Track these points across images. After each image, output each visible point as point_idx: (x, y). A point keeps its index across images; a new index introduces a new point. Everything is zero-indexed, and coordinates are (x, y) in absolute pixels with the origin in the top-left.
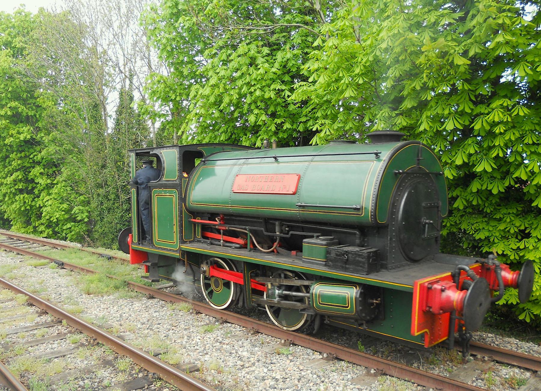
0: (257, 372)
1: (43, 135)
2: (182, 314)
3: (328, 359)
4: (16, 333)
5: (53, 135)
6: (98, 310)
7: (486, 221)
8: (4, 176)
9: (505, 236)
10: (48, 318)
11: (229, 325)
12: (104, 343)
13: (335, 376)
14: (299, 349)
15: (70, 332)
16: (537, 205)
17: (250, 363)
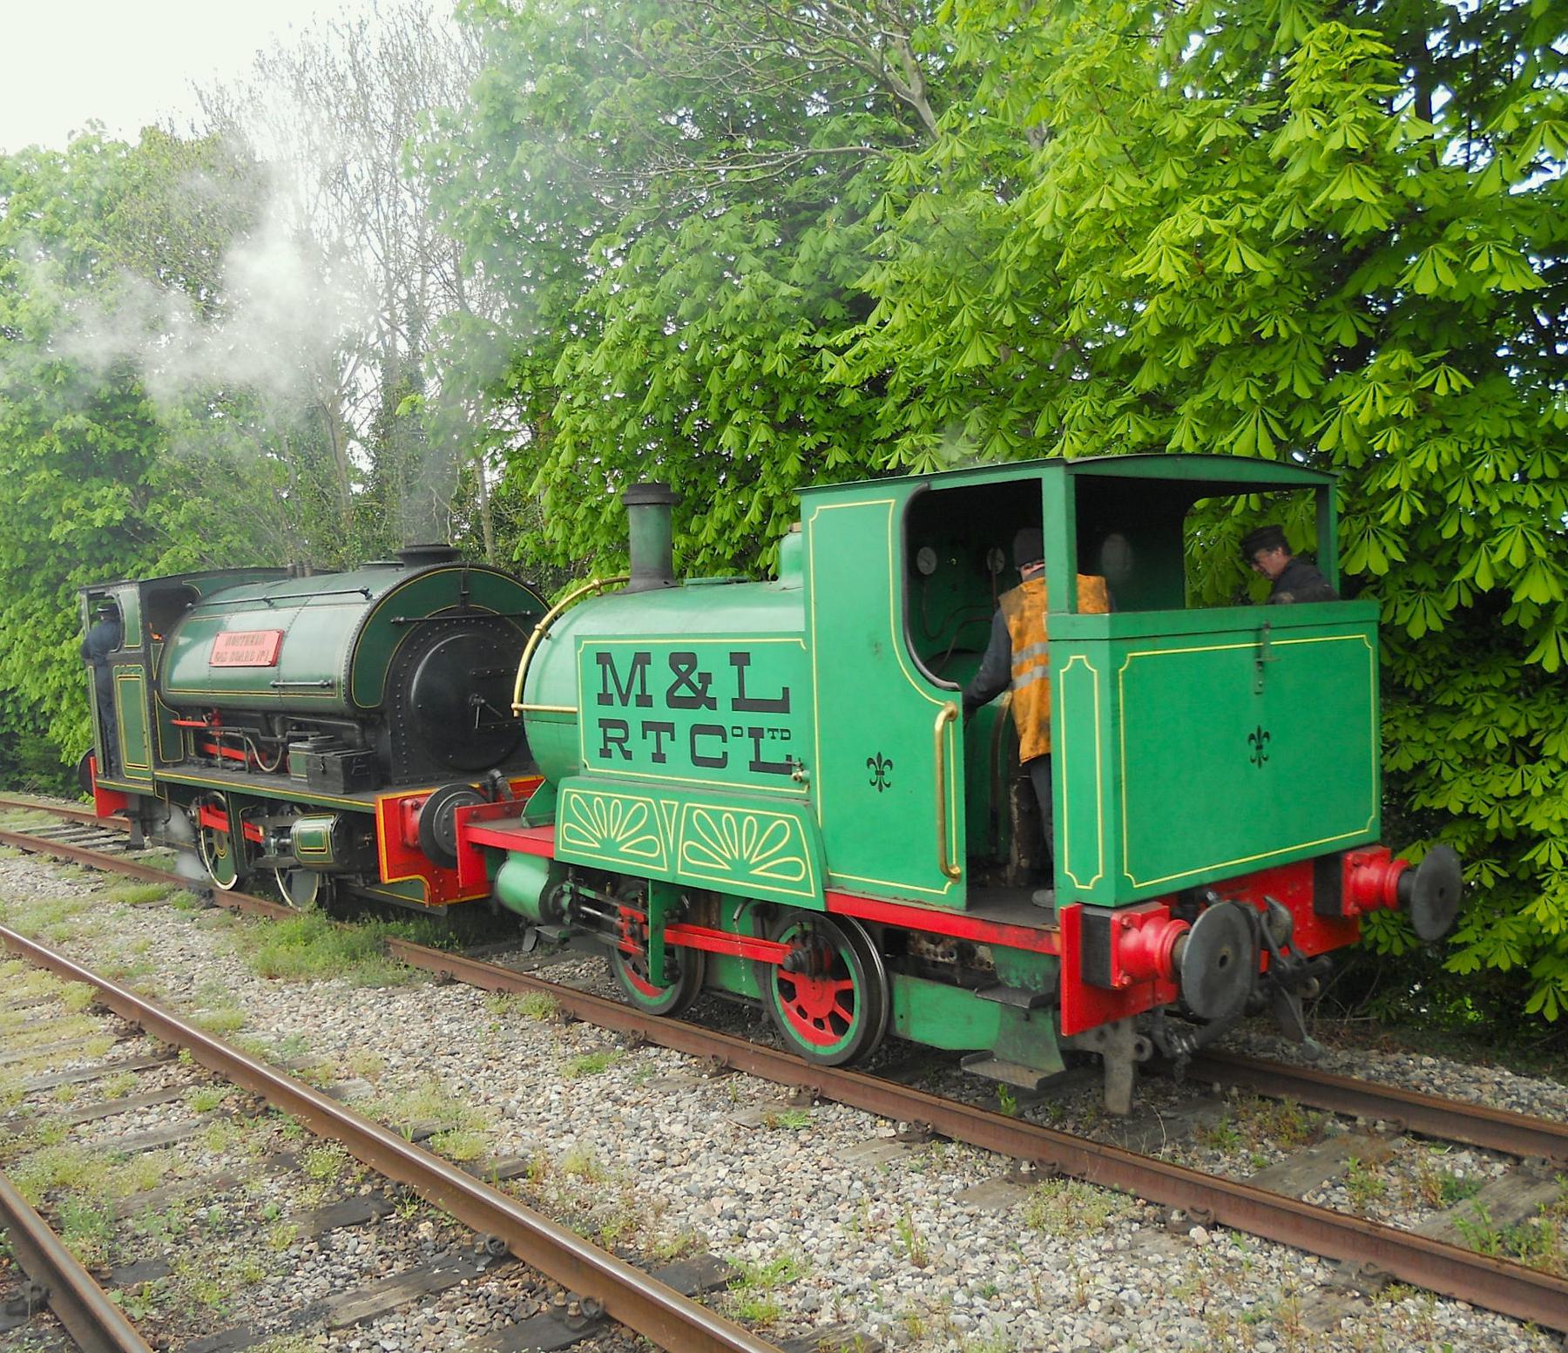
0: (696, 1177)
1: (160, 509)
2: (523, 1024)
3: (908, 1140)
4: (50, 1089)
5: (188, 509)
6: (288, 1020)
7: (1417, 716)
8: (54, 637)
9: (1475, 760)
10: (143, 1047)
11: (653, 1051)
12: (281, 1108)
13: (916, 1185)
14: (832, 1113)
15: (198, 1082)
16: (1539, 663)
17: (685, 1153)
